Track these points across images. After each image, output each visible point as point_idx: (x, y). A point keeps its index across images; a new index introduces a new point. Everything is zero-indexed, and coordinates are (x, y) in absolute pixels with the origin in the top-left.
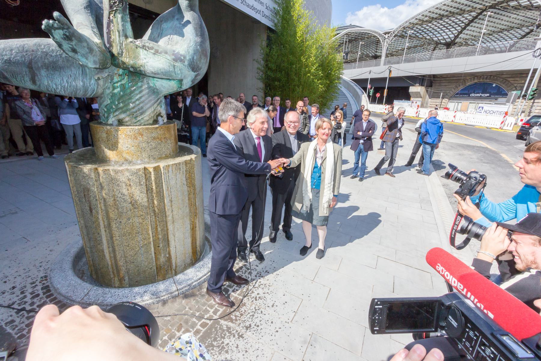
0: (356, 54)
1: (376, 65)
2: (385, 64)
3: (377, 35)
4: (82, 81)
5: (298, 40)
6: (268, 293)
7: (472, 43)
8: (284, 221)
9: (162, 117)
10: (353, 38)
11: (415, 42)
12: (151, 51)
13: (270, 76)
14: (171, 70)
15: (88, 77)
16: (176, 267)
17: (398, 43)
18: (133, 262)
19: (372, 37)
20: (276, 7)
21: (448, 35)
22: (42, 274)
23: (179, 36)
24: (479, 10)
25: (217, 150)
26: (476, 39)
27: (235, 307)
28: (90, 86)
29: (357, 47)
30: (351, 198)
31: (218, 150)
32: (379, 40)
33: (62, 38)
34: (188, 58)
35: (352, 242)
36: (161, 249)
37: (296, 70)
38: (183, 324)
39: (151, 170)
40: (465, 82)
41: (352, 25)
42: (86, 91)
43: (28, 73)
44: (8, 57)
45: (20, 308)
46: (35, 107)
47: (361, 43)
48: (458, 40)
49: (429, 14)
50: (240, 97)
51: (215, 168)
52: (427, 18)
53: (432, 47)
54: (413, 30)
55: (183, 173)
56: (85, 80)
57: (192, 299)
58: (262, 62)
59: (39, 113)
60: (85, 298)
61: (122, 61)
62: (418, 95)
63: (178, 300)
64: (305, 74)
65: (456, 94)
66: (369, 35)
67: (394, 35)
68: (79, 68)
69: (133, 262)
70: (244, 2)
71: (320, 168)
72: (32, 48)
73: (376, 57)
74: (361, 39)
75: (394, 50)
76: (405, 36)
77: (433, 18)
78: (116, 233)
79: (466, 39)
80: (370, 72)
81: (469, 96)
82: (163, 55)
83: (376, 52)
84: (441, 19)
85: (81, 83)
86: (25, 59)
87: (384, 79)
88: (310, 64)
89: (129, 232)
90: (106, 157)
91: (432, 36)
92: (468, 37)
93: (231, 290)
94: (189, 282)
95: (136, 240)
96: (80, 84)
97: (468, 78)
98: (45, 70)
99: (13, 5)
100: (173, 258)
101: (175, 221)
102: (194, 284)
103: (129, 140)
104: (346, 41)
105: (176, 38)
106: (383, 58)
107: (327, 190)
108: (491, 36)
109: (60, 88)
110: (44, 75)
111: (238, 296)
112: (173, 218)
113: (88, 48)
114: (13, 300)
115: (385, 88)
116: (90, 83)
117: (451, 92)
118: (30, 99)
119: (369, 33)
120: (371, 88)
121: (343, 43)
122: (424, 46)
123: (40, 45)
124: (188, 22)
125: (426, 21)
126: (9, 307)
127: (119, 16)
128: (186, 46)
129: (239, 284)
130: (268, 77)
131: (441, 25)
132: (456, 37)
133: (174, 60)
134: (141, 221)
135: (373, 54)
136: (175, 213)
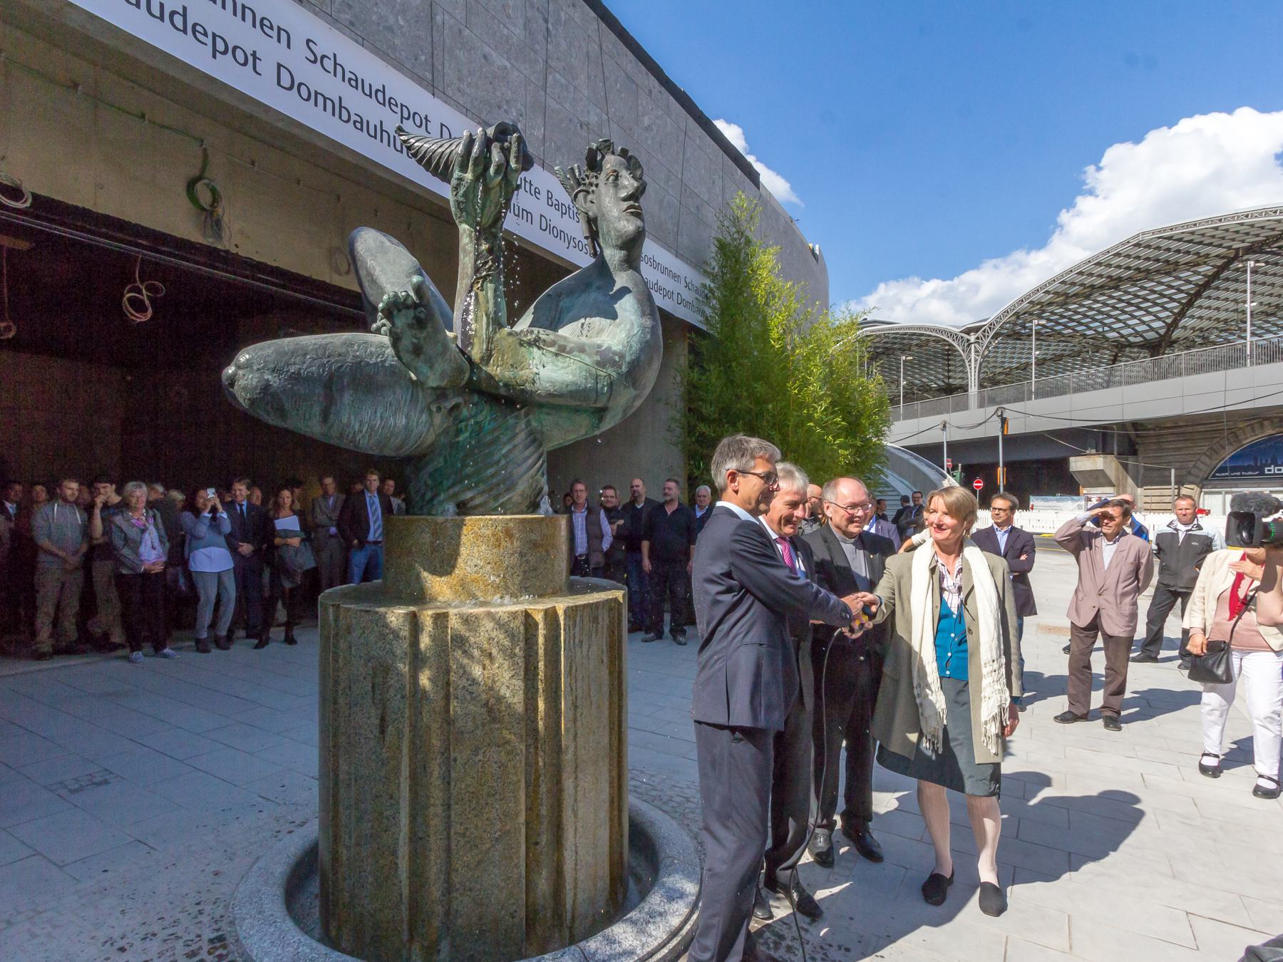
2: (981, 405)
4: (407, 417)
5: (773, 346)
7: (1221, 337)
8: (849, 799)
10: (878, 348)
11: (1054, 348)
12: (549, 349)
14: (589, 385)
15: (419, 408)
17: (1006, 353)
18: (470, 890)
19: (932, 344)
20: (708, 282)
21: (1150, 323)
22: (208, 934)
23: (606, 317)
24: (1217, 259)
25: (738, 546)
26: (1232, 327)
28: (417, 426)
31: (744, 548)
34: (628, 359)
35: (1076, 870)
36: (541, 853)
39: (539, 618)
40: (1237, 437)
43: (321, 399)
44: (298, 366)
46: (152, 528)
48: (1177, 334)
49: (1079, 279)
50: (632, 487)
51: (728, 599)
52: (1076, 289)
53: (1107, 354)
54: (1042, 318)
59: (157, 544)
61: (487, 373)
62: (1098, 478)
64: (800, 424)
65: (1219, 471)
67: (991, 334)
68: (408, 389)
69: (470, 890)
71: (960, 616)
72: (339, 350)
74: (903, 351)
75: (999, 370)
76: (1022, 334)
77: (1092, 287)
78: (437, 795)
79: (1201, 330)
80: (944, 426)
81: (1262, 473)
82: (576, 356)
83: (949, 377)
84: (1117, 288)
86: (324, 371)
89: (471, 789)
91: (1100, 330)
92: (1205, 324)
97: (1242, 425)
98: (351, 392)
99: (138, 320)
100: (568, 887)
105: (597, 321)
106: (973, 390)
108: (1272, 319)
110: (347, 402)
112: (575, 754)
115: (997, 465)
116: (417, 422)
117: (1202, 466)
118: (144, 511)
119: (922, 335)
122: (1083, 355)
123: (352, 345)
124: (624, 291)
125: (1076, 295)
127: (490, 287)
128: (624, 335)
131: (1121, 301)
132: (1172, 326)
133: (598, 363)
134: (504, 757)
135: (941, 383)
136: (581, 742)
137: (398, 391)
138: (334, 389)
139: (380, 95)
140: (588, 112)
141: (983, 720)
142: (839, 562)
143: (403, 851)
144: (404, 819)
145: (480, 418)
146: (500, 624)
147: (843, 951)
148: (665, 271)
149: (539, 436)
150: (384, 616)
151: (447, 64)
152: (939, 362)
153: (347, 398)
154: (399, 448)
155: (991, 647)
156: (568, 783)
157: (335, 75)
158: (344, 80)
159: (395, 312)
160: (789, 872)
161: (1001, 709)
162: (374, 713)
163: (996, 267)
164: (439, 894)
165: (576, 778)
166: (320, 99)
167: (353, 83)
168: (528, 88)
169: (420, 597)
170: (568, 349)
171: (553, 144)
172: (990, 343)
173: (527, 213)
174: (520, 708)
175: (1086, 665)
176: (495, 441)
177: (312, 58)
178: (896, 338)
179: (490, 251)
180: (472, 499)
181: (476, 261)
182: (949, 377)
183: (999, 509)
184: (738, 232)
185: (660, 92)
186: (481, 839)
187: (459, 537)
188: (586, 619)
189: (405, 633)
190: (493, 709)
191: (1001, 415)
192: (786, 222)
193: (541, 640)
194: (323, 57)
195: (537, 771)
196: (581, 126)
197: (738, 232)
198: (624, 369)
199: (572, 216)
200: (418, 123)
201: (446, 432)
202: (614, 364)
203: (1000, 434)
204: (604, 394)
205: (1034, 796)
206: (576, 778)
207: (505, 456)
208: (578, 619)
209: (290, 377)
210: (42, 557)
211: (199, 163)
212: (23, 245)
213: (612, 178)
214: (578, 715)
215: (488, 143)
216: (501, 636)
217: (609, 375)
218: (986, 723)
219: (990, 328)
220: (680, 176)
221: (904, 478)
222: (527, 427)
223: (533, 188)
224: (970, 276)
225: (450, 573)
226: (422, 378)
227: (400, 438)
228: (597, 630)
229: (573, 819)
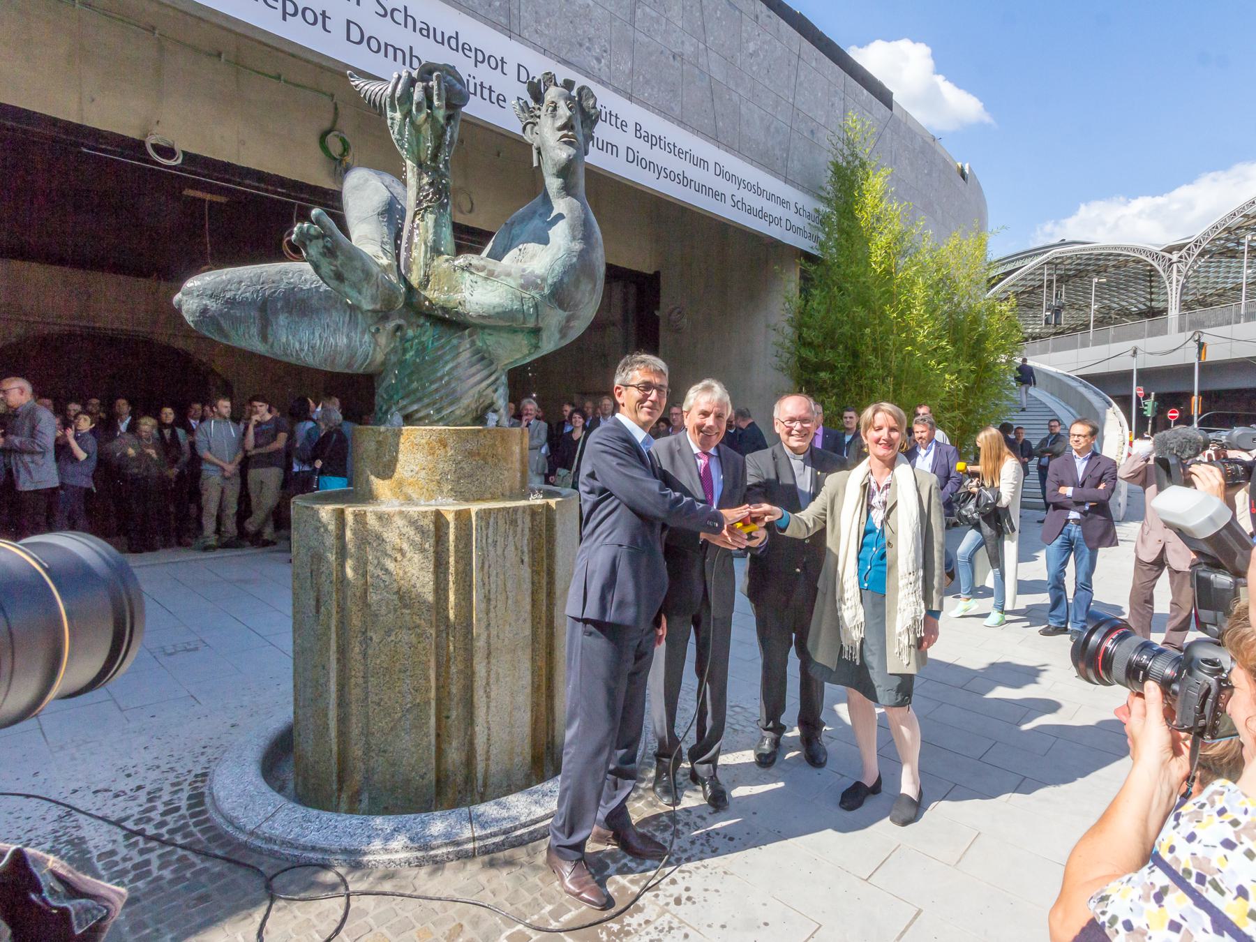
0: (1087, 310)
1: (1152, 334)
2: (1181, 330)
3: (1143, 257)
4: (348, 336)
6: (717, 891)
9: (495, 411)
10: (1070, 270)
12: (480, 274)
13: (806, 360)
15: (359, 329)
16: (486, 778)
17: (1219, 272)
20: (823, 208)
27: (613, 911)
28: (361, 345)
29: (1087, 293)
30: (1044, 679)
32: (1153, 270)
33: (321, 254)
34: (550, 281)
37: (874, 340)
38: (467, 927)
39: (450, 518)
41: (1067, 240)
42: (352, 357)
44: (233, 293)
45: (135, 828)
47: (1096, 280)
55: (523, 535)
56: (353, 334)
57: (505, 872)
58: (789, 330)
60: (265, 824)
63: (473, 867)
66: (1121, 258)
67: (1197, 251)
68: (345, 312)
70: (740, 204)
71: (883, 531)
73: (1154, 313)
74: (1098, 273)
75: (1209, 292)
76: (1237, 252)
78: (356, 666)
80: (1135, 352)
83: (1152, 300)
85: (345, 340)
87: (1187, 370)
88: (913, 324)
89: (385, 665)
90: (371, 491)
93: (613, 867)
94: (507, 825)
95: (397, 689)
96: (342, 341)
101: (493, 654)
102: (518, 833)
103: (419, 456)
104: (1050, 282)
105: (532, 247)
106: (1174, 312)
107: (906, 591)
109: (306, 348)
110: (282, 323)
111: (628, 885)
112: (489, 644)
113: (363, 271)
114: (129, 812)
116: (361, 341)
119: (1120, 255)
120: (1147, 396)
121: (1041, 286)
124: (560, 217)
126: (118, 823)
129: (638, 855)
130: (803, 364)
133: (522, 286)
134: (414, 639)
135: (1144, 307)
137: (334, 313)
138: (269, 312)
139: (453, 42)
140: (683, 43)
141: (897, 632)
142: (786, 480)
143: (333, 713)
144: (333, 686)
145: (424, 339)
146: (413, 523)
147: (726, 840)
148: (771, 197)
149: (486, 355)
150: (317, 512)
151: (522, 7)
152: (1140, 284)
153: (282, 319)
154: (349, 365)
155: (907, 559)
156: (480, 668)
157: (406, 26)
158: (415, 30)
159: (308, 243)
160: (706, 766)
161: (915, 620)
162: (313, 594)
163: (1214, 180)
164: (360, 753)
165: (489, 663)
166: (390, 50)
167: (425, 32)
168: (614, 24)
169: (368, 496)
170: (496, 273)
171: (641, 77)
172: (1195, 261)
173: (612, 146)
174: (430, 598)
175: (1148, 598)
176: (435, 361)
177: (382, 12)
178: (1090, 259)
179: (431, 184)
180: (417, 411)
181: (418, 193)
182: (1152, 300)
183: (1079, 436)
184: (852, 155)
185: (769, 17)
186: (394, 708)
187: (398, 445)
188: (501, 522)
189: (332, 527)
190: (405, 598)
191: (1199, 340)
192: (925, 142)
193: (452, 537)
194: (393, 10)
195: (448, 654)
196: (674, 57)
197: (852, 155)
198: (546, 291)
199: (662, 146)
200: (493, 65)
201: (394, 350)
202: (536, 286)
203: (1196, 361)
204: (531, 315)
205: (1030, 720)
206: (489, 663)
207: (449, 373)
208: (492, 520)
209: (227, 302)
210: (205, 466)
211: (330, 116)
212: (222, 199)
213: (550, 109)
214: (492, 607)
215: (412, 82)
216: (411, 532)
217: (533, 297)
218: (900, 635)
219: (1196, 246)
220: (791, 100)
221: (1071, 407)
222: (471, 346)
223: (619, 122)
224: (1184, 192)
225: (391, 477)
226: (356, 303)
227: (345, 356)
228: (515, 532)
229: (484, 699)
